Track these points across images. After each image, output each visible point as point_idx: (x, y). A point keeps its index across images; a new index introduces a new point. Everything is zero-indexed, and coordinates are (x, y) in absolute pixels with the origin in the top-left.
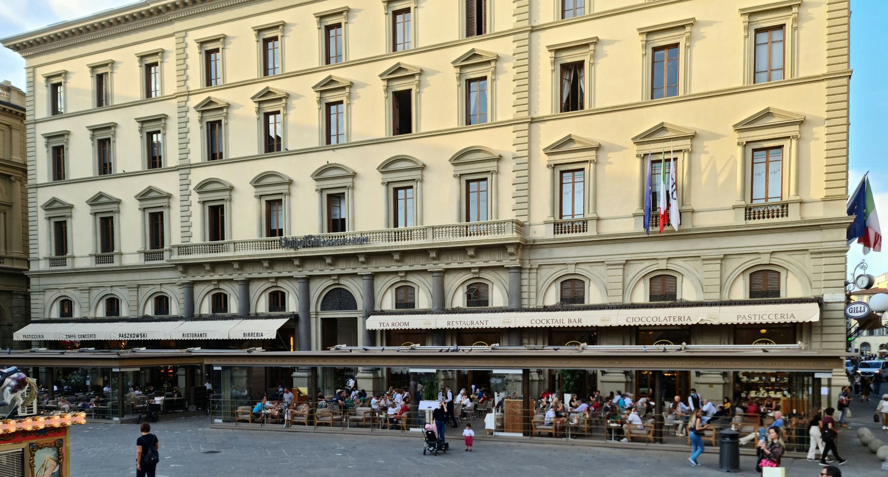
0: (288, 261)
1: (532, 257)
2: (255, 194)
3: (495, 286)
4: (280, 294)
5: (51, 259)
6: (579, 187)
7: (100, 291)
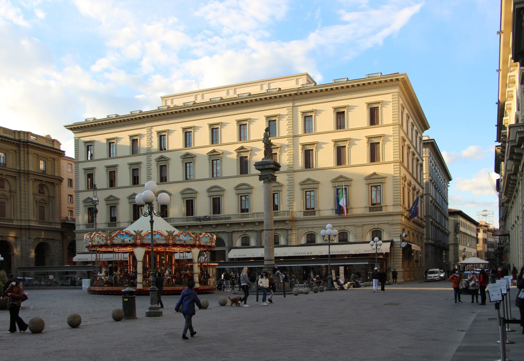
3: (252, 238)
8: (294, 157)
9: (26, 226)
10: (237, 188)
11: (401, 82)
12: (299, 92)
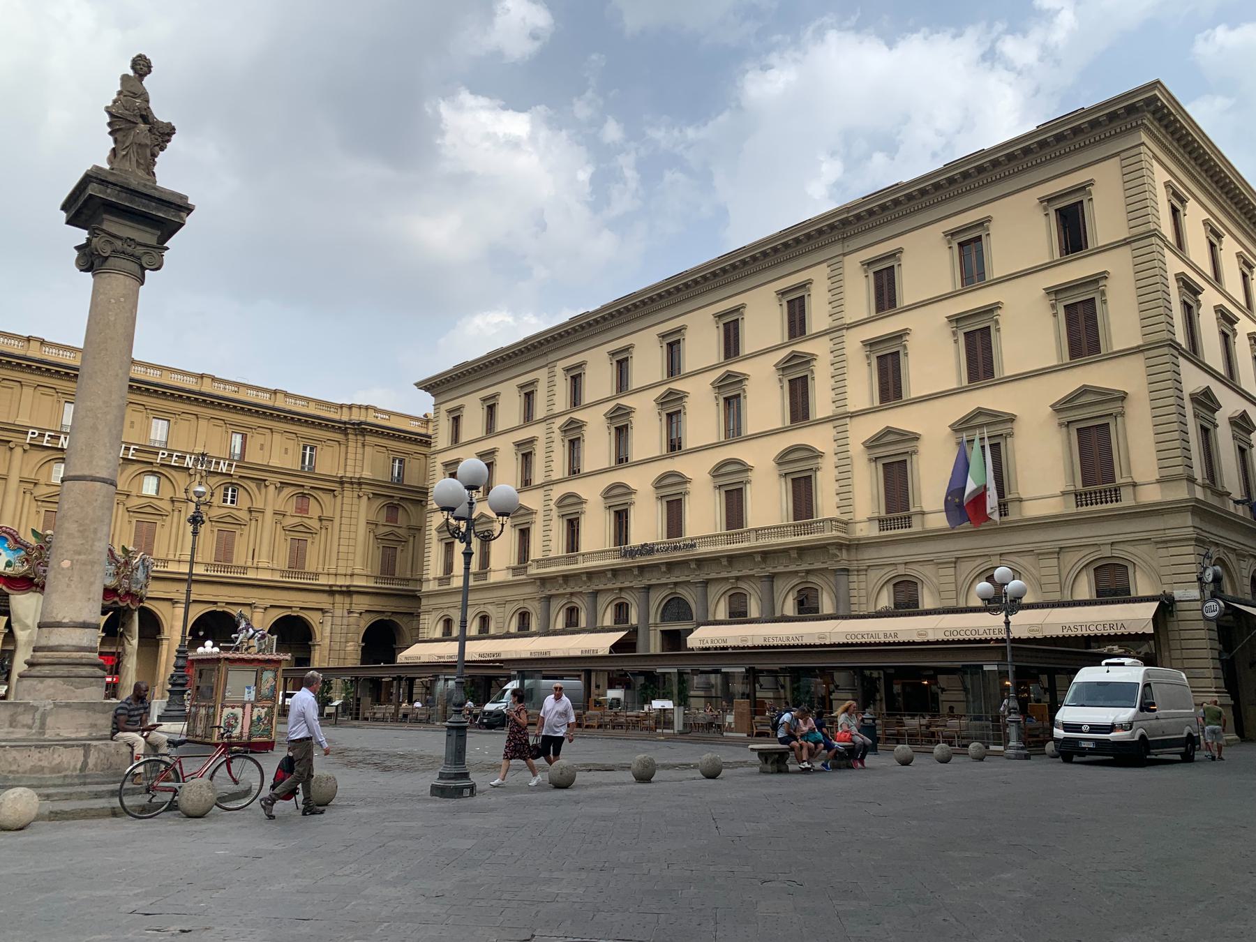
0: (628, 570)
3: (926, 591)
7: (883, 572)
9: (341, 586)
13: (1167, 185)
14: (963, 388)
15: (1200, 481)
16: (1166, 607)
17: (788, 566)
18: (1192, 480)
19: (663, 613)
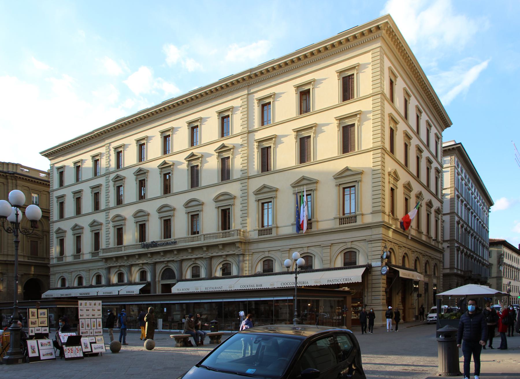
0: (144, 255)
1: (250, 248)
2: (185, 212)
4: (145, 272)
5: (92, 253)
6: (353, 196)
8: (249, 159)
9: (11, 261)
10: (186, 205)
11: (384, 32)
12: (252, 73)
13: (390, 68)
14: (259, 175)
15: (387, 213)
16: (369, 269)
17: (218, 253)
18: (384, 213)
19: (162, 275)
